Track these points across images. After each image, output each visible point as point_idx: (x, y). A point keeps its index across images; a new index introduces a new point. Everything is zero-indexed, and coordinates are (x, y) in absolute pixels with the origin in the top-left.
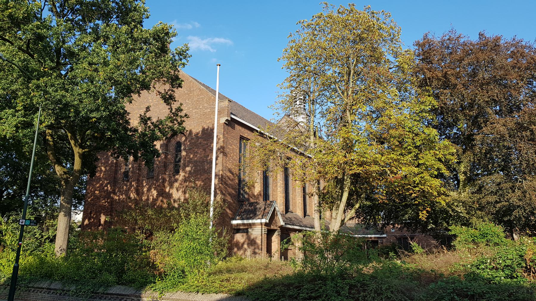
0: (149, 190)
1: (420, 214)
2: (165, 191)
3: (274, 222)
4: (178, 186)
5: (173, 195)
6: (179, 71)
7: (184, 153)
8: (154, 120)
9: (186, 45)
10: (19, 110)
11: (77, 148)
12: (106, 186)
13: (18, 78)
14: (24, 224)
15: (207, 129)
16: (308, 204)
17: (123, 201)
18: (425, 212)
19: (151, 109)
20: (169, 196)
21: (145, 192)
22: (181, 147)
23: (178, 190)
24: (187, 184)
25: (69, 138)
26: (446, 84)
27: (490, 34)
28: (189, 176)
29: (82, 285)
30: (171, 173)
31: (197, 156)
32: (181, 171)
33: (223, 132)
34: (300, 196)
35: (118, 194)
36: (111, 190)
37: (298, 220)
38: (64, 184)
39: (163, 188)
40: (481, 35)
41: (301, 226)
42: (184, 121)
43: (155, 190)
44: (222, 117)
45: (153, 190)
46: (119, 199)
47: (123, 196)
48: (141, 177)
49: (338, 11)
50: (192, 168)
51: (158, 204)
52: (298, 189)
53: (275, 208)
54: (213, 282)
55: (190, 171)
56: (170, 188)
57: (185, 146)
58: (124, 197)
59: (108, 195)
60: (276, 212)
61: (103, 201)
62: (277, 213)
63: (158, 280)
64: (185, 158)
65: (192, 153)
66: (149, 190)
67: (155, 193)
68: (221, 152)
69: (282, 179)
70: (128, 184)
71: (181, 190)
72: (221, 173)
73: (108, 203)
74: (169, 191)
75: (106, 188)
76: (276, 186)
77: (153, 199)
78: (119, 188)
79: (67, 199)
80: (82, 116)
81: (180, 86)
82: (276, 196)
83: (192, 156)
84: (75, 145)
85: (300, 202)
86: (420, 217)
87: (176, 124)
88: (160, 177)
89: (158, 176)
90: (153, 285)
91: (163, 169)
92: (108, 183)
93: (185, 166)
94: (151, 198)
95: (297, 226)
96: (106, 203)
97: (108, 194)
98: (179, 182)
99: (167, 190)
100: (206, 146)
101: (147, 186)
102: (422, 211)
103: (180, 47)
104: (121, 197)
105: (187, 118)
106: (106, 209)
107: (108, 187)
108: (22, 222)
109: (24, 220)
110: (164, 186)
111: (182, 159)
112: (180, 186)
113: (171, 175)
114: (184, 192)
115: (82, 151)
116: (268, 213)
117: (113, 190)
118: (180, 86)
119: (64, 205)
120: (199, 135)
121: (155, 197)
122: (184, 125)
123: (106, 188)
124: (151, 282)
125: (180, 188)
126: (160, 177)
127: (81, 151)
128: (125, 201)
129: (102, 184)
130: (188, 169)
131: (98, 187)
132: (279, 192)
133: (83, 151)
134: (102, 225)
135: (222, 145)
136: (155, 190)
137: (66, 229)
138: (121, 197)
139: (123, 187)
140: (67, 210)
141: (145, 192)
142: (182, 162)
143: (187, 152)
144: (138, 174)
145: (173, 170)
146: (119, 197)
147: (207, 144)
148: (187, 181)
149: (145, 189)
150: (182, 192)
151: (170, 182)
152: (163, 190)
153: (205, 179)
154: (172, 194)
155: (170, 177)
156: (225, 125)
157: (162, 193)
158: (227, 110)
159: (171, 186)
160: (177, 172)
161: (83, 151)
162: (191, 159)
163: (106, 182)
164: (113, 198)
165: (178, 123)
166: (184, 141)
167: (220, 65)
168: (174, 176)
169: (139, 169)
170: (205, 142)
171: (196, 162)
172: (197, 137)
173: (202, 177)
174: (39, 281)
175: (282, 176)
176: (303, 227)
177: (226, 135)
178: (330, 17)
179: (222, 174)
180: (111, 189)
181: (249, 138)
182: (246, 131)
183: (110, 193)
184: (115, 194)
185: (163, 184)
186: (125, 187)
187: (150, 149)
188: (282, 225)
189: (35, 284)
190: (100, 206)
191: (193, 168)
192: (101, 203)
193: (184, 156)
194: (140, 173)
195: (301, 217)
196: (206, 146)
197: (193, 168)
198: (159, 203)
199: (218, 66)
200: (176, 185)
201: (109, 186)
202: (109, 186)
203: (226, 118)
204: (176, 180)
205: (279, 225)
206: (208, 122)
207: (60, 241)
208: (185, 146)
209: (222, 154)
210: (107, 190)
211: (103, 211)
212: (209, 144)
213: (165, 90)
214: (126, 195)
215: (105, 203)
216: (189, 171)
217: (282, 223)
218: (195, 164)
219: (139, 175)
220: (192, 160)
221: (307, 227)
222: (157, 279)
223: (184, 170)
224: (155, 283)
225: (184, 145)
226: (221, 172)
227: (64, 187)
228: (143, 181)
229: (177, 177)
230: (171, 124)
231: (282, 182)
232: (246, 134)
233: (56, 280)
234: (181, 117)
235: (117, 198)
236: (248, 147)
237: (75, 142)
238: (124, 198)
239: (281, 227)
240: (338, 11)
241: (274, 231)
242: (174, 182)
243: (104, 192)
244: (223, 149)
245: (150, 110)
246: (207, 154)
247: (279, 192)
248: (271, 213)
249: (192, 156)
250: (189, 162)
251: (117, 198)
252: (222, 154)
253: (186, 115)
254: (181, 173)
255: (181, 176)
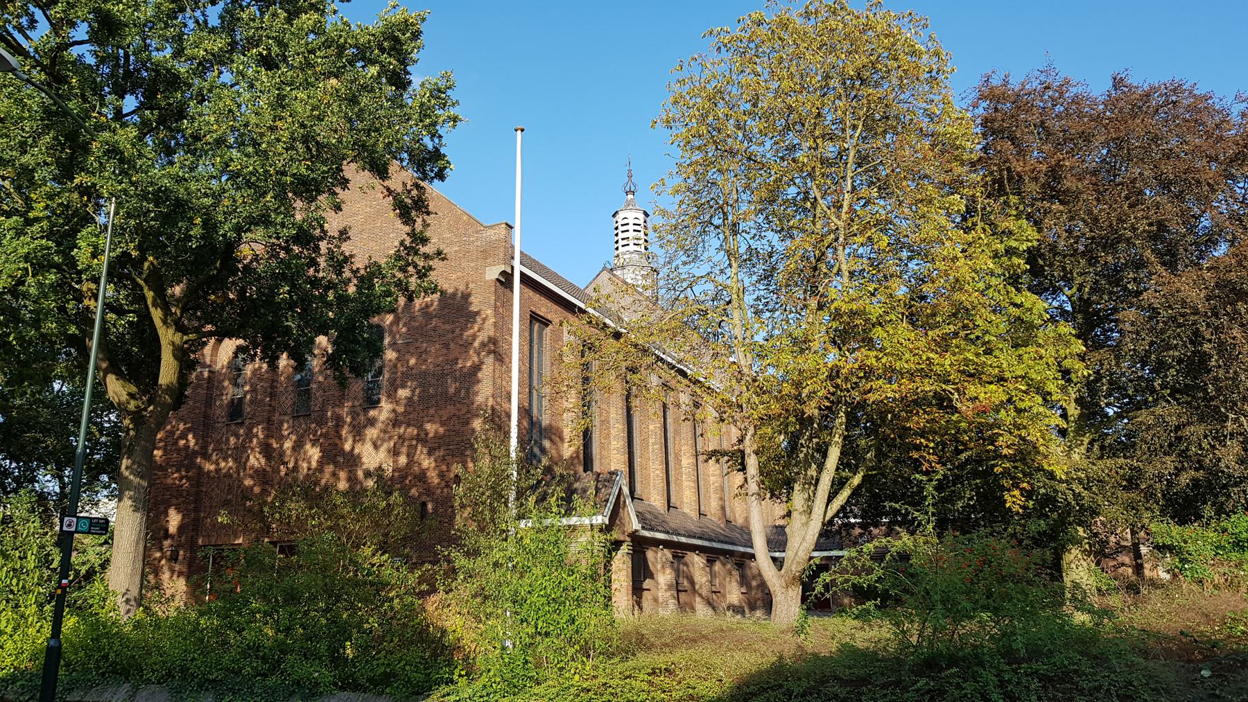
0: (298, 447)
1: (1007, 497)
2: (343, 449)
3: (617, 522)
4: (375, 436)
5: (364, 460)
6: (440, 137)
7: (390, 355)
8: (359, 263)
9: (446, 77)
10: (37, 220)
11: (171, 331)
12: (184, 436)
13: (39, 135)
14: (73, 529)
15: (454, 294)
16: (672, 479)
17: (228, 475)
18: (1016, 493)
19: (350, 234)
20: (352, 461)
21: (289, 452)
22: (382, 338)
23: (376, 447)
24: (402, 430)
25: (149, 302)
26: (1053, 191)
27: (1142, 78)
28: (406, 411)
29: (234, 693)
30: (357, 403)
31: (426, 360)
32: (384, 399)
33: (493, 302)
34: (659, 459)
35: (214, 457)
36: (196, 448)
37: (656, 517)
38: (131, 426)
39: (337, 441)
40: (1118, 83)
41: (667, 533)
42: (430, 268)
43: (313, 445)
44: (490, 265)
45: (308, 446)
46: (218, 470)
47: (227, 462)
48: (277, 415)
49: (807, 7)
50: (413, 391)
51: (323, 482)
52: (653, 444)
53: (620, 489)
54: (629, 677)
55: (410, 399)
56: (354, 441)
57: (394, 337)
58: (231, 464)
59: (187, 460)
60: (622, 499)
61: (175, 475)
62: (625, 502)
63: (460, 676)
64: (395, 366)
65: (412, 355)
66: (298, 447)
67: (314, 453)
68: (489, 352)
69: (621, 420)
70: (242, 431)
71: (386, 445)
72: (491, 402)
73: (188, 479)
74: (353, 448)
75: (182, 442)
76: (608, 435)
77: (309, 469)
78: (219, 442)
79: (140, 465)
80: (224, 235)
81: (441, 176)
82: (607, 460)
83: (412, 361)
84: (165, 322)
85: (658, 476)
86: (1008, 505)
87: (412, 275)
88: (329, 414)
89: (323, 410)
90: (444, 689)
91: (337, 394)
92: (189, 430)
93: (394, 386)
94: (305, 465)
95: (661, 532)
96: (184, 481)
97: (190, 455)
98: (379, 426)
99: (347, 447)
100: (450, 336)
101: (294, 438)
102: (1009, 490)
103: (434, 79)
104: (223, 464)
105: (443, 259)
106: (185, 494)
107: (187, 440)
108: (70, 525)
109: (75, 519)
110: (340, 437)
111: (387, 369)
112: (382, 435)
113: (358, 409)
114: (395, 453)
115: (182, 338)
116: (607, 501)
117: (202, 448)
118: (441, 176)
119: (131, 481)
120: (432, 309)
121: (314, 464)
122: (433, 276)
123: (182, 442)
124: (439, 682)
125: (383, 440)
126: (329, 414)
127: (178, 338)
128: (235, 475)
129: (172, 433)
130: (403, 393)
131: (161, 440)
132: (615, 452)
133: (185, 338)
134: (172, 537)
135: (492, 333)
136: (313, 445)
137: (137, 543)
138: (223, 464)
139: (228, 440)
140: (139, 493)
141: (289, 452)
142: (387, 376)
143: (398, 351)
144: (270, 406)
145: (361, 395)
146: (218, 464)
147: (453, 332)
148: (402, 422)
149: (288, 445)
150: (389, 451)
151: (354, 427)
152: (337, 445)
153: (449, 419)
154: (359, 456)
155: (354, 414)
156: (498, 284)
157: (334, 455)
158: (502, 249)
159: (358, 434)
160: (374, 404)
161: (185, 338)
162: (412, 369)
163: (181, 426)
164: (200, 468)
165: (418, 272)
166: (392, 324)
167: (522, 130)
168: (366, 410)
169: (271, 394)
170: (448, 327)
171: (424, 375)
172: (427, 313)
173: (440, 412)
174: (97, 685)
175: (620, 412)
176: (672, 534)
177: (501, 310)
178: (784, 25)
179: (492, 406)
180: (196, 444)
181: (549, 318)
182: (544, 301)
183: (195, 454)
184: (207, 457)
185: (337, 432)
186: (232, 440)
187: (362, 336)
188: (636, 531)
189: (86, 694)
190: (168, 488)
191: (417, 391)
192: (169, 481)
193: (390, 360)
194: (273, 403)
195: (662, 512)
196: (450, 336)
197: (417, 391)
198: (326, 478)
199: (519, 132)
200: (372, 433)
201: (190, 437)
202: (190, 437)
203: (502, 268)
204: (372, 422)
205: (630, 531)
206: (454, 276)
207: (122, 576)
208: (394, 337)
209: (492, 356)
210: (187, 447)
211: (174, 501)
212: (457, 331)
213: (404, 184)
214: (235, 460)
215: (181, 479)
216: (406, 398)
217: (636, 525)
218: (422, 378)
219: (273, 410)
220: (414, 371)
221: (679, 535)
222: (457, 672)
223: (391, 396)
224: (452, 681)
225: (391, 332)
226: (491, 399)
227: (132, 433)
228: (281, 423)
229: (372, 413)
230: (400, 275)
231: (621, 427)
232: (543, 309)
233: (148, 682)
234: (427, 257)
235: (212, 467)
236: (547, 341)
237: (166, 315)
238: (230, 468)
239: (634, 536)
240: (807, 7)
241: (617, 544)
242: (365, 427)
243: (179, 450)
244: (494, 344)
245: (349, 238)
246: (452, 357)
247: (615, 452)
248: (612, 499)
249: (412, 361)
250: (407, 375)
251: (212, 467)
252: (492, 356)
253: (439, 253)
254: (383, 404)
255: (385, 410)
